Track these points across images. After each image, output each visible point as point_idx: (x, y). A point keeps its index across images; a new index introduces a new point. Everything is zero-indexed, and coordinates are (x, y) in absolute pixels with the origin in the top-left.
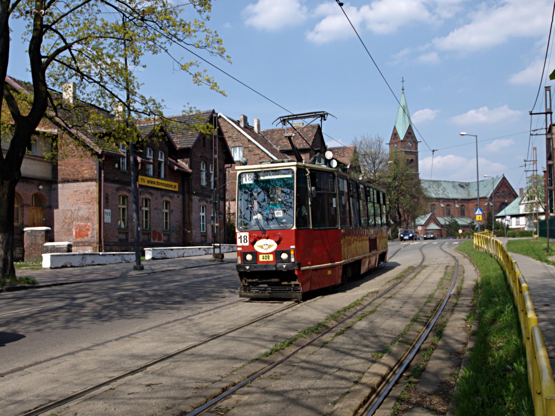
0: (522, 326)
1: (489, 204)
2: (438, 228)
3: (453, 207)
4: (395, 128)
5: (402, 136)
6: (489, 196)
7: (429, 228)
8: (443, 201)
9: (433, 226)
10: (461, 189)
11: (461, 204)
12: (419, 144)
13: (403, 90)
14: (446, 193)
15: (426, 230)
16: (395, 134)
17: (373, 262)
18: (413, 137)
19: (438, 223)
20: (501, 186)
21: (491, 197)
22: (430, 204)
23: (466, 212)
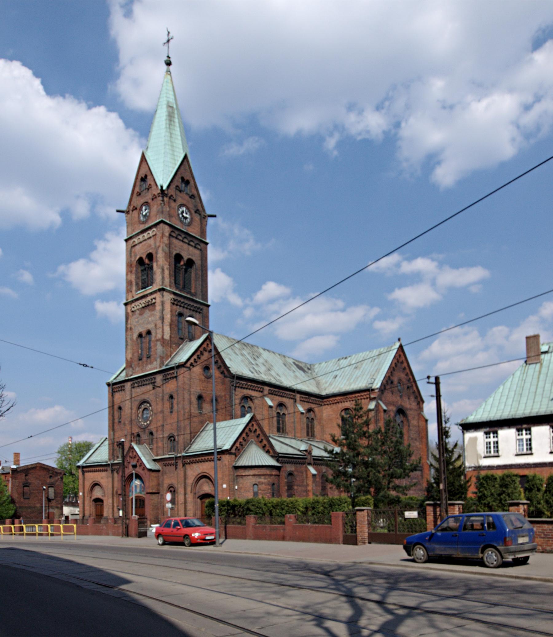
0: (72, 581)
1: (377, 405)
2: (272, 462)
3: (291, 410)
4: (143, 159)
5: (163, 177)
6: (377, 385)
7: (243, 462)
8: (271, 393)
9: (255, 456)
10: (301, 372)
11: (308, 406)
12: (210, 221)
13: (169, 64)
14: (273, 373)
15: (237, 468)
16: (144, 177)
17: (144, 185)
18: (192, 197)
19: (269, 449)
20: (394, 369)
21: (383, 388)
22: (240, 393)
23: (317, 429)
